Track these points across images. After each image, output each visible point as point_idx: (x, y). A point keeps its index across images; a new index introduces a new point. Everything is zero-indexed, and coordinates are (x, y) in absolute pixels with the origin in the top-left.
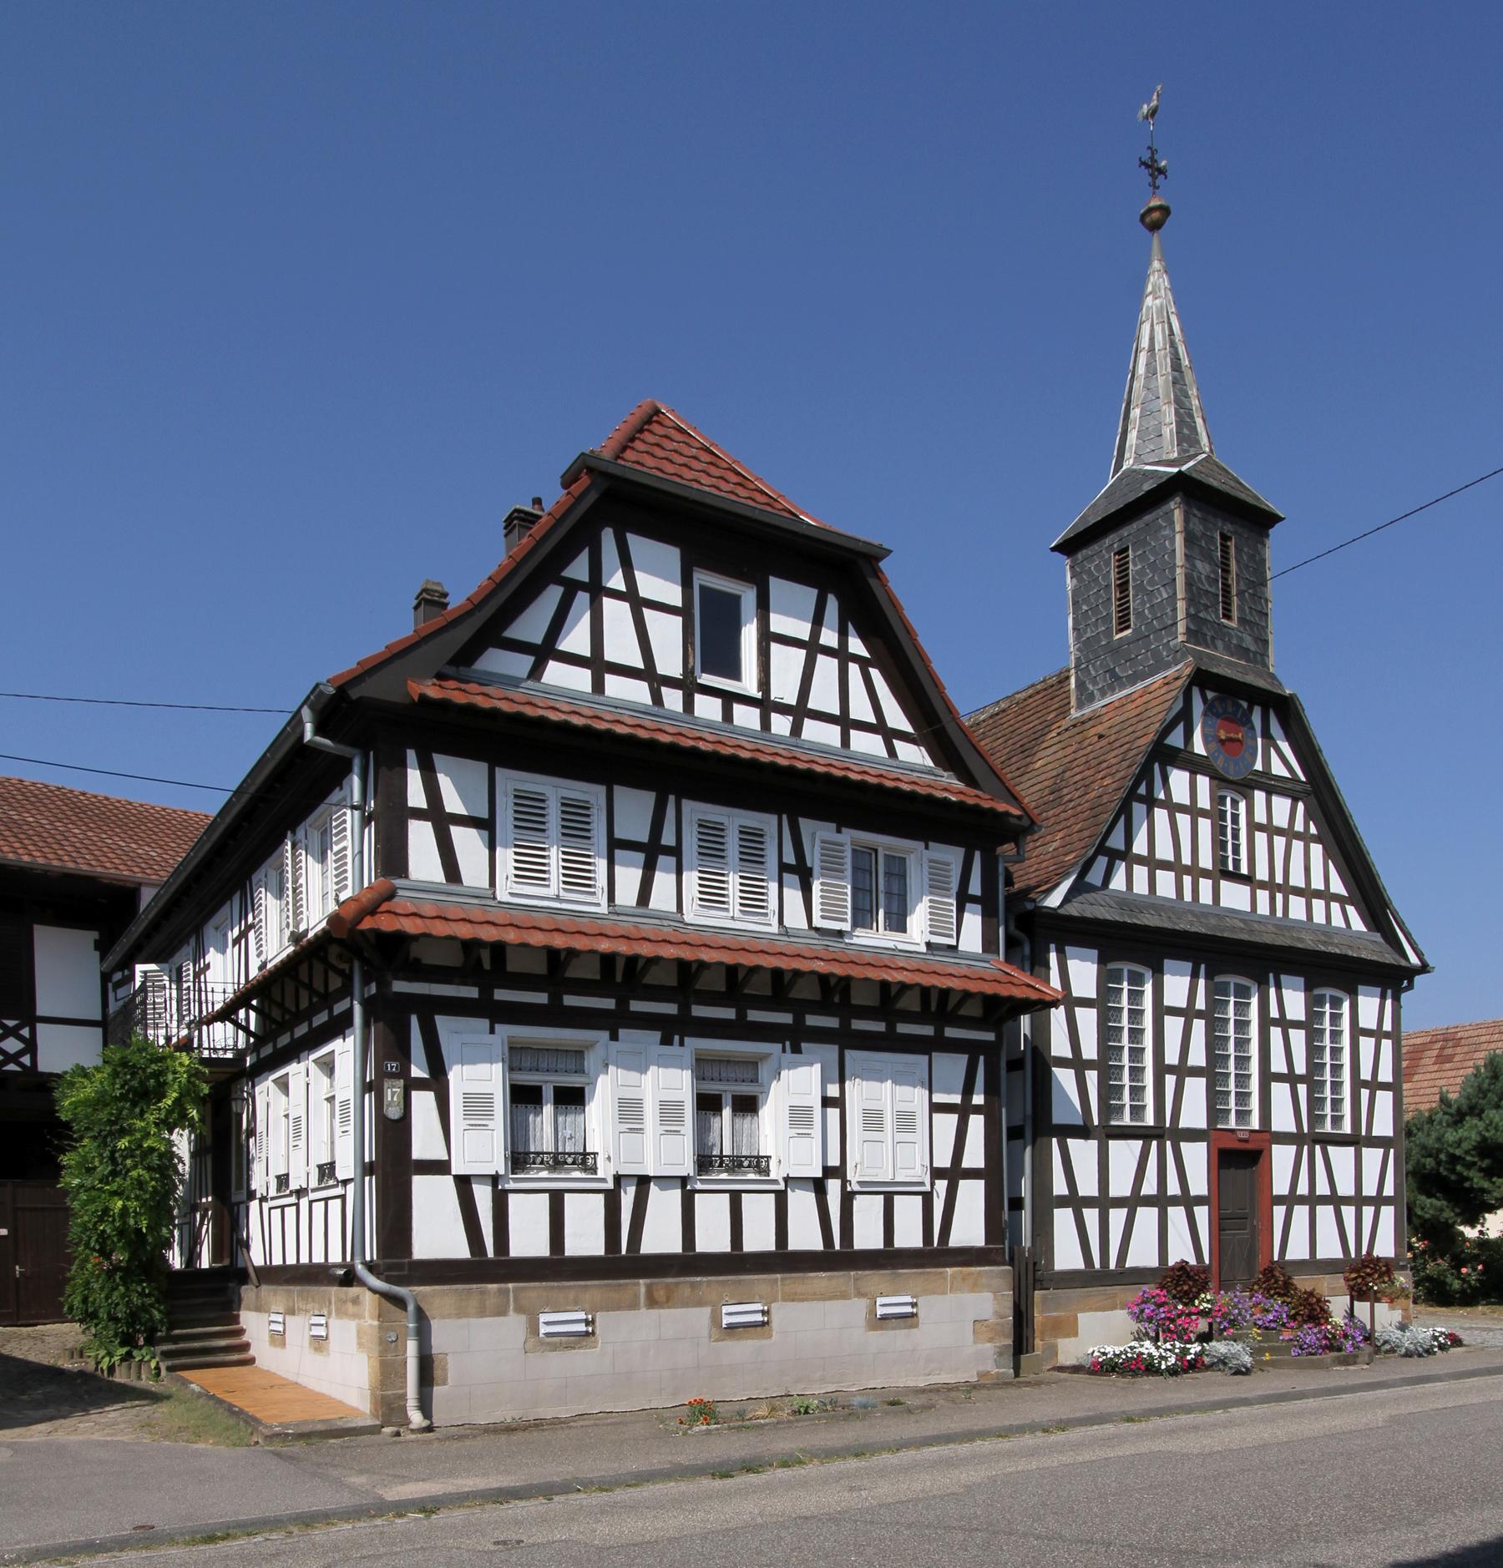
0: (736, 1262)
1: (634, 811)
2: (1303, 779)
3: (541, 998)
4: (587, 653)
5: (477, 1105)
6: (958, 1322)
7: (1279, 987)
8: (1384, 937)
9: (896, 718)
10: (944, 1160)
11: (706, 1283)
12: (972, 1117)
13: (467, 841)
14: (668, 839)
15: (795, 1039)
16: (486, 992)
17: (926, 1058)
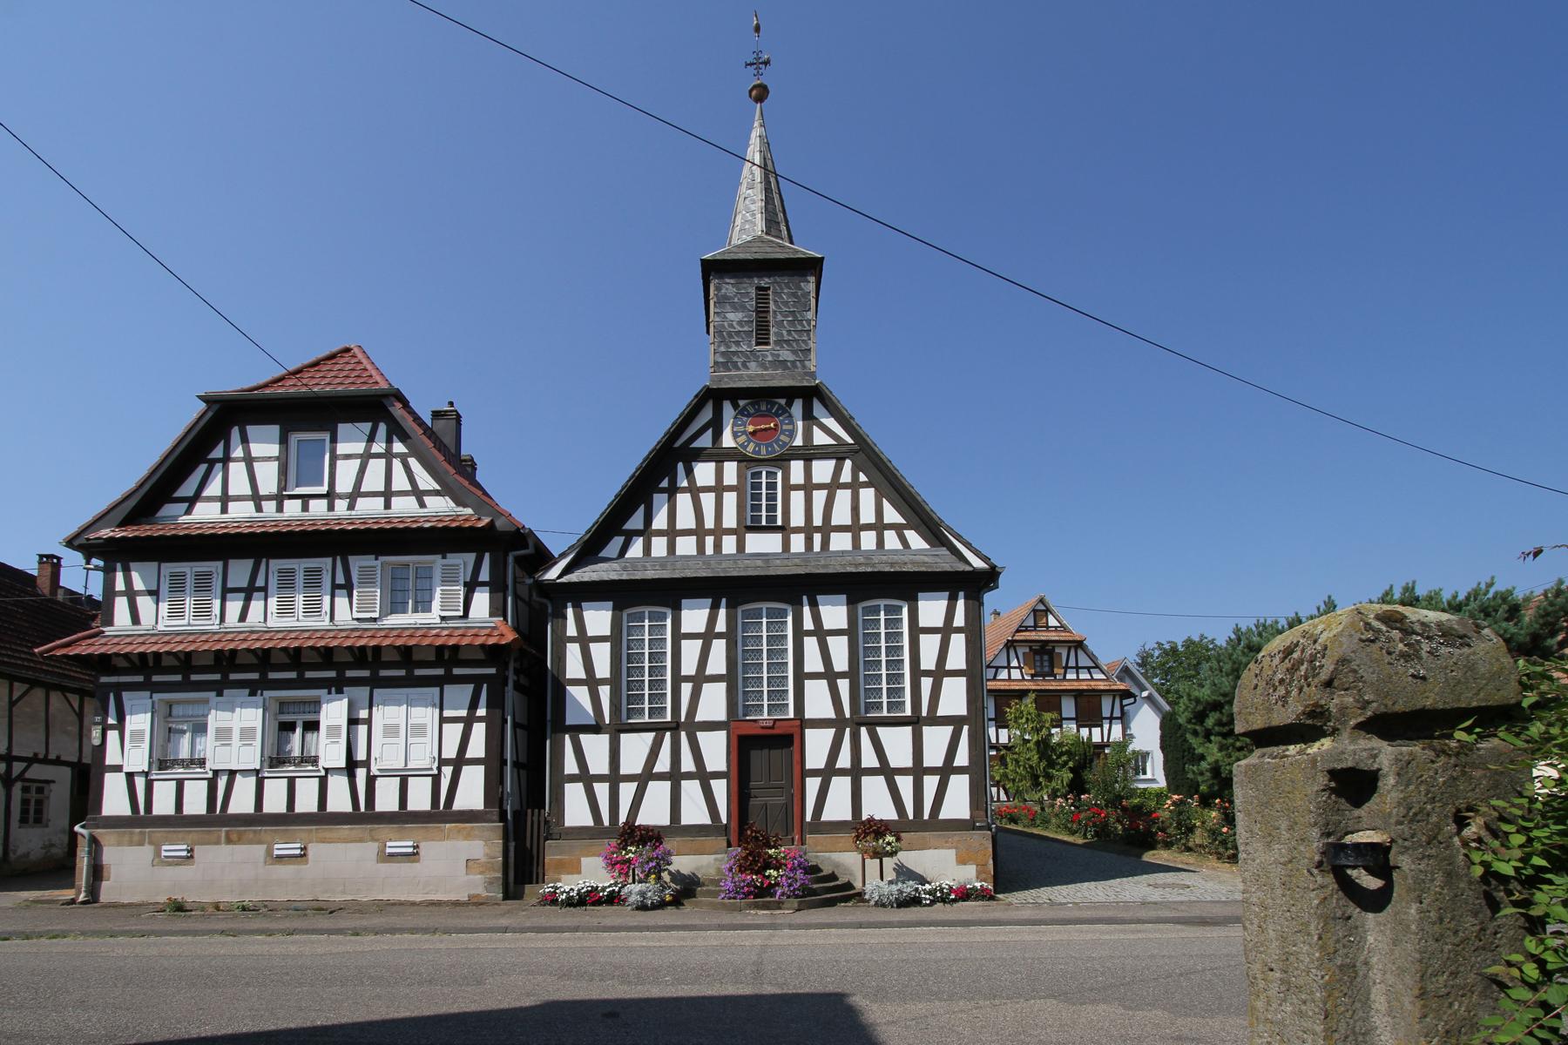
0: (290, 819)
1: (240, 571)
2: (850, 441)
5: (137, 735)
6: (459, 863)
7: (814, 605)
10: (450, 752)
15: (337, 686)
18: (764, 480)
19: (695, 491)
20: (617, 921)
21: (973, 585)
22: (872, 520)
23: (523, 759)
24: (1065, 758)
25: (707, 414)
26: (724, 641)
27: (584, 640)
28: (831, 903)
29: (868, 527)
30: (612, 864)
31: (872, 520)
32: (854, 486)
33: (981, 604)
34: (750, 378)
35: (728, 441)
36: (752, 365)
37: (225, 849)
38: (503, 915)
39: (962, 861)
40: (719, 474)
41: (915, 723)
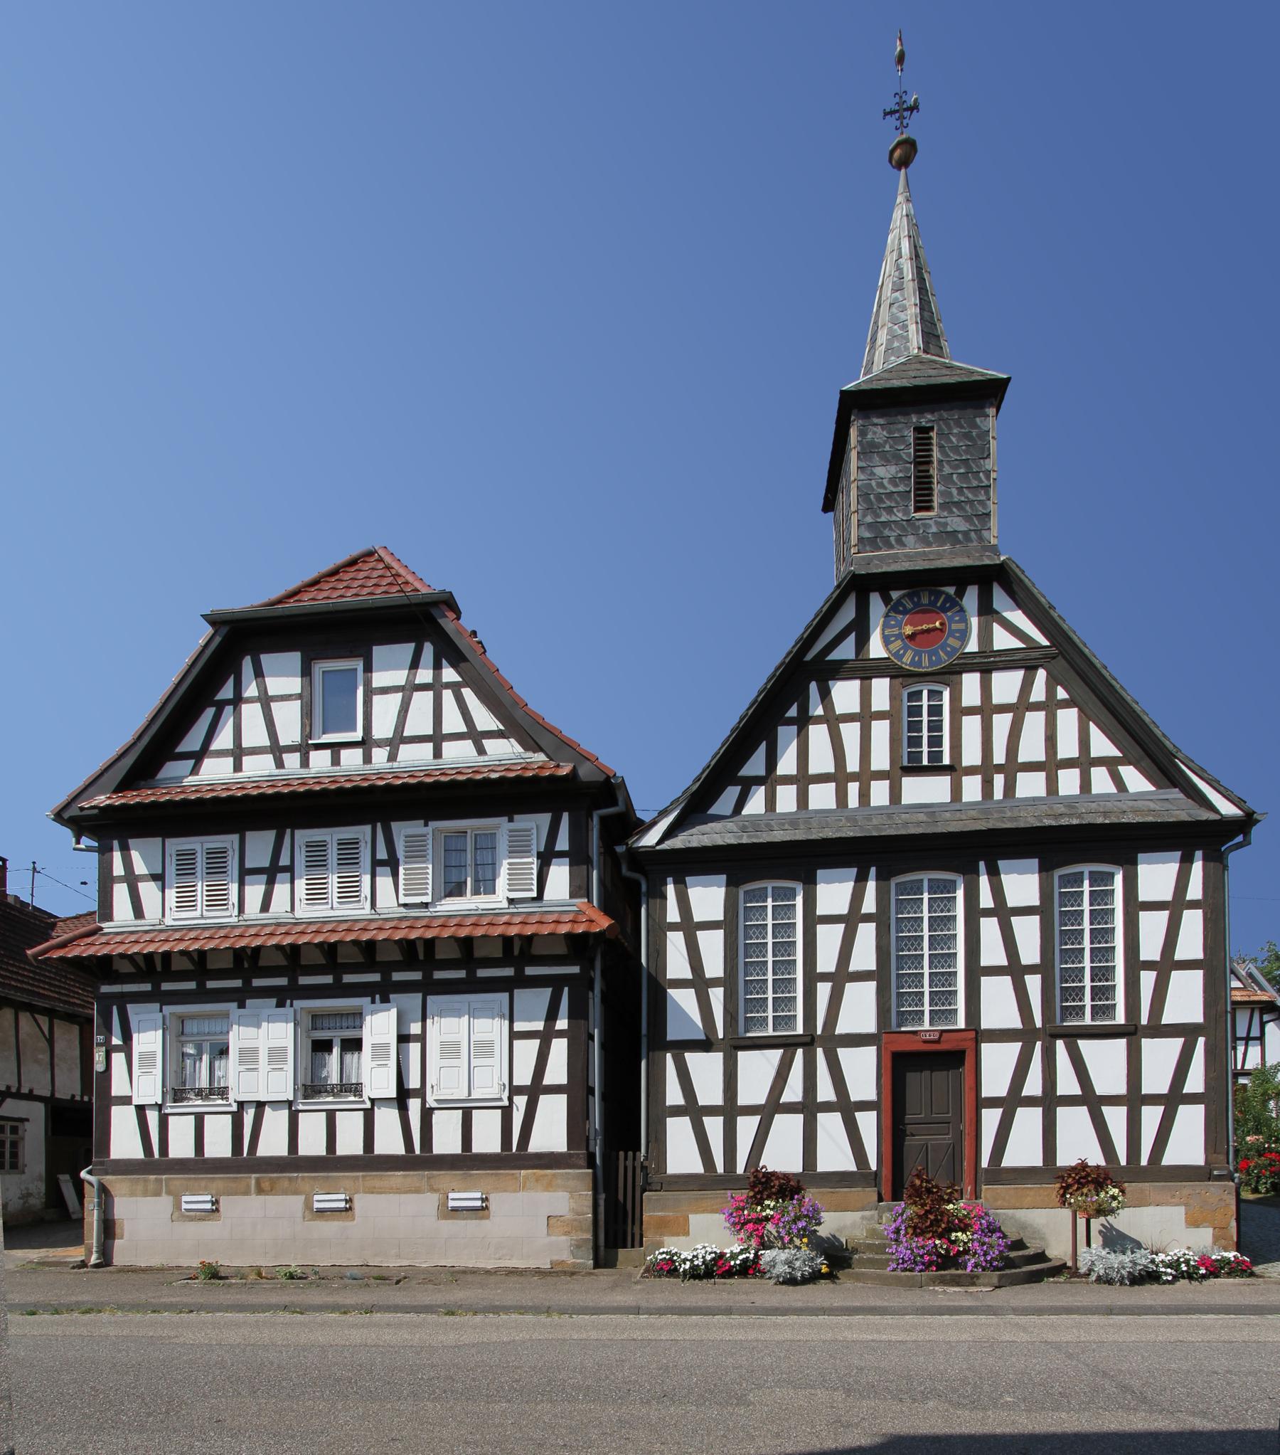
1: (260, 846)
2: (1045, 643)
3: (461, 974)
4: (464, 729)
5: (147, 1058)
6: (540, 1219)
7: (994, 873)
9: (485, 720)
10: (524, 1077)
11: (303, 1178)
12: (554, 1041)
13: (148, 891)
14: (284, 861)
15: (382, 993)
16: (156, 986)
17: (506, 995)
19: (833, 721)
25: (848, 613)
27: (689, 927)
30: (739, 1225)
34: (909, 557)
35: (876, 649)
36: (910, 540)
37: (255, 1201)
39: (1193, 1222)
41: (1132, 1033)
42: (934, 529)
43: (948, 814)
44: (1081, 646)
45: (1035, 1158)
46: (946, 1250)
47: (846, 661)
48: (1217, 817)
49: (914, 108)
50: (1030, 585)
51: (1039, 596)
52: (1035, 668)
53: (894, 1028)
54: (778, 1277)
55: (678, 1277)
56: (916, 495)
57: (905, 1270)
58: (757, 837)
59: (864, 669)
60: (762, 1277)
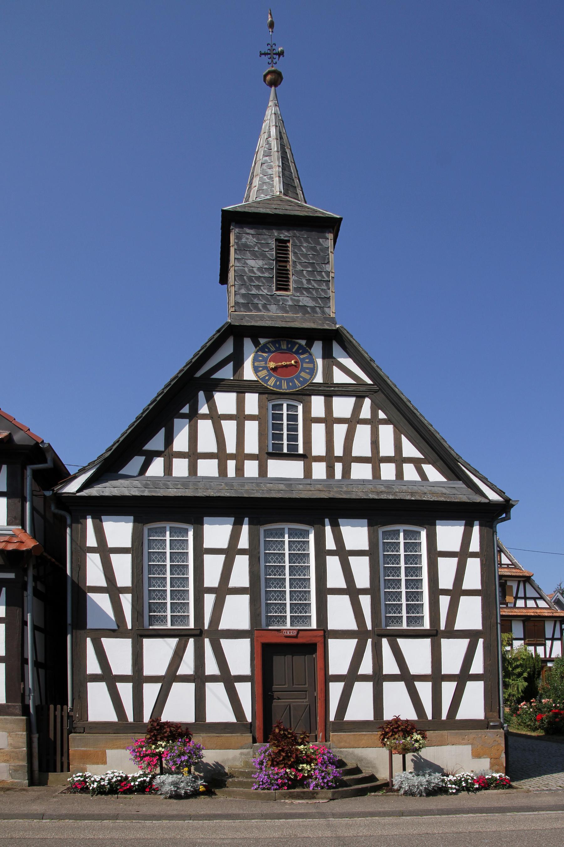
2: (369, 382)
7: (335, 526)
8: (465, 483)
18: (285, 412)
19: (216, 418)
20: (155, 810)
21: (487, 514)
22: (392, 453)
23: (41, 659)
24: (519, 670)
25: (228, 349)
26: (478, 560)
27: (104, 551)
28: (362, 793)
29: (388, 460)
30: (140, 757)
31: (392, 453)
32: (374, 422)
33: (494, 532)
34: (271, 318)
35: (249, 374)
36: (273, 308)
38: (34, 800)
39: (477, 755)
40: (240, 404)
41: (435, 635)
42: (290, 303)
43: (301, 486)
44: (393, 386)
45: (368, 715)
46: (295, 775)
47: (223, 380)
48: (487, 501)
49: (281, 54)
50: (356, 345)
51: (363, 352)
52: (364, 397)
53: (264, 626)
54: (167, 793)
55: (89, 793)
56: (277, 281)
57: (264, 789)
58: (155, 492)
59: (239, 386)
60: (156, 793)
